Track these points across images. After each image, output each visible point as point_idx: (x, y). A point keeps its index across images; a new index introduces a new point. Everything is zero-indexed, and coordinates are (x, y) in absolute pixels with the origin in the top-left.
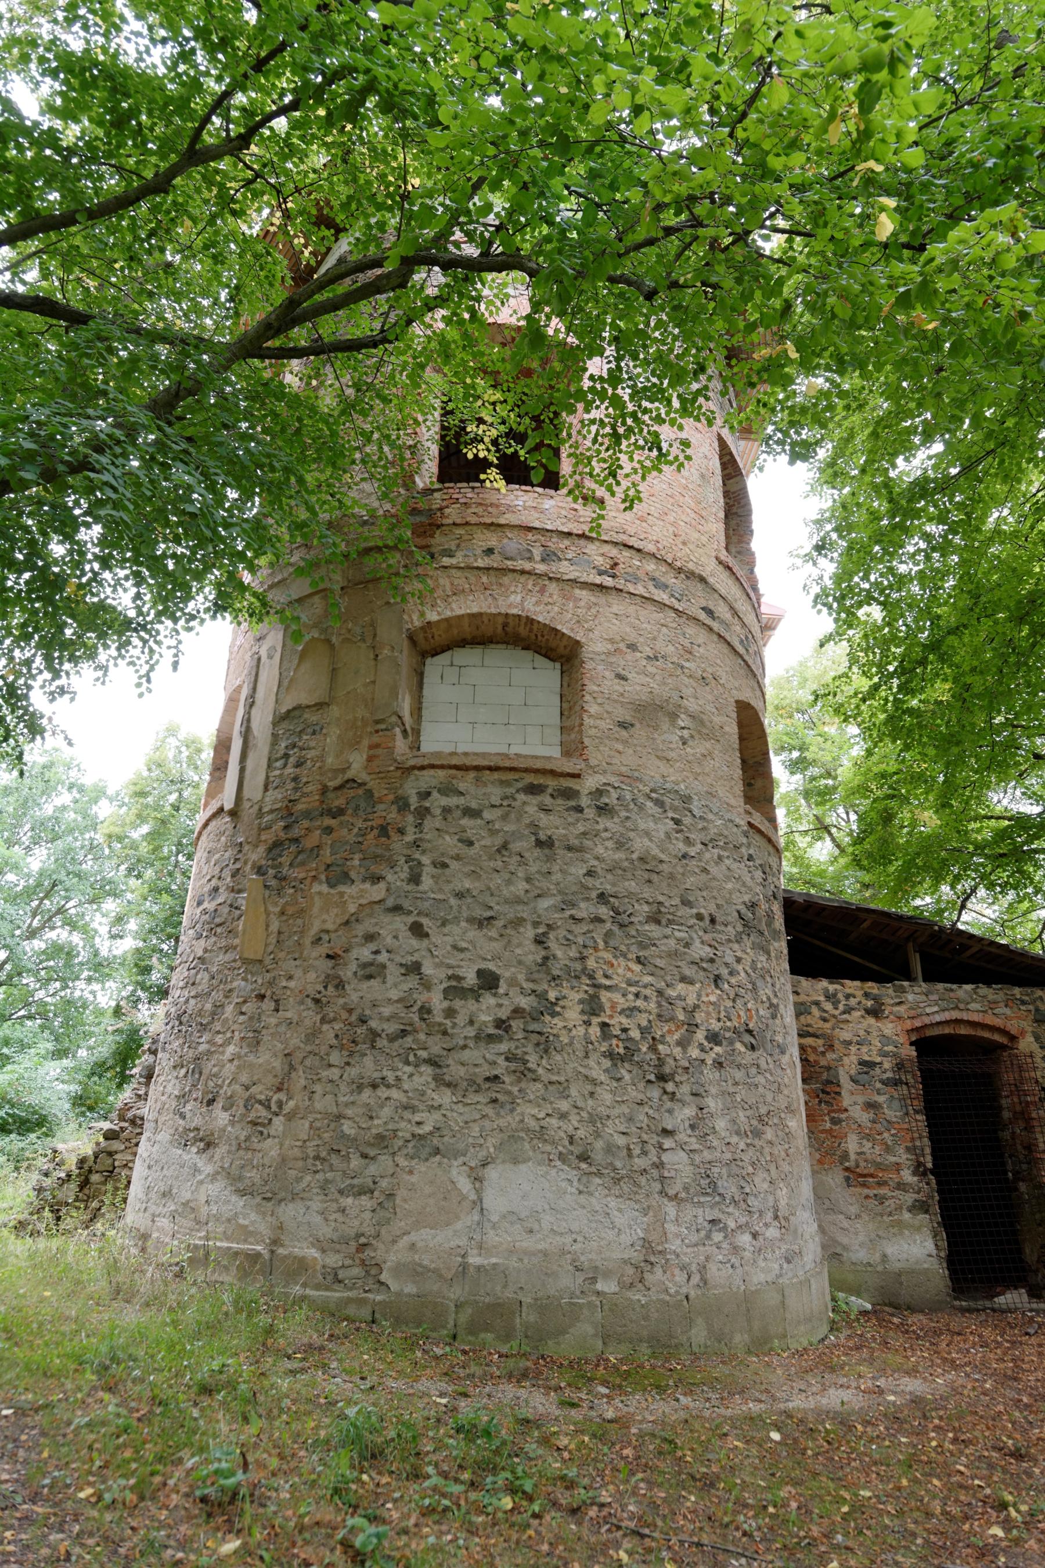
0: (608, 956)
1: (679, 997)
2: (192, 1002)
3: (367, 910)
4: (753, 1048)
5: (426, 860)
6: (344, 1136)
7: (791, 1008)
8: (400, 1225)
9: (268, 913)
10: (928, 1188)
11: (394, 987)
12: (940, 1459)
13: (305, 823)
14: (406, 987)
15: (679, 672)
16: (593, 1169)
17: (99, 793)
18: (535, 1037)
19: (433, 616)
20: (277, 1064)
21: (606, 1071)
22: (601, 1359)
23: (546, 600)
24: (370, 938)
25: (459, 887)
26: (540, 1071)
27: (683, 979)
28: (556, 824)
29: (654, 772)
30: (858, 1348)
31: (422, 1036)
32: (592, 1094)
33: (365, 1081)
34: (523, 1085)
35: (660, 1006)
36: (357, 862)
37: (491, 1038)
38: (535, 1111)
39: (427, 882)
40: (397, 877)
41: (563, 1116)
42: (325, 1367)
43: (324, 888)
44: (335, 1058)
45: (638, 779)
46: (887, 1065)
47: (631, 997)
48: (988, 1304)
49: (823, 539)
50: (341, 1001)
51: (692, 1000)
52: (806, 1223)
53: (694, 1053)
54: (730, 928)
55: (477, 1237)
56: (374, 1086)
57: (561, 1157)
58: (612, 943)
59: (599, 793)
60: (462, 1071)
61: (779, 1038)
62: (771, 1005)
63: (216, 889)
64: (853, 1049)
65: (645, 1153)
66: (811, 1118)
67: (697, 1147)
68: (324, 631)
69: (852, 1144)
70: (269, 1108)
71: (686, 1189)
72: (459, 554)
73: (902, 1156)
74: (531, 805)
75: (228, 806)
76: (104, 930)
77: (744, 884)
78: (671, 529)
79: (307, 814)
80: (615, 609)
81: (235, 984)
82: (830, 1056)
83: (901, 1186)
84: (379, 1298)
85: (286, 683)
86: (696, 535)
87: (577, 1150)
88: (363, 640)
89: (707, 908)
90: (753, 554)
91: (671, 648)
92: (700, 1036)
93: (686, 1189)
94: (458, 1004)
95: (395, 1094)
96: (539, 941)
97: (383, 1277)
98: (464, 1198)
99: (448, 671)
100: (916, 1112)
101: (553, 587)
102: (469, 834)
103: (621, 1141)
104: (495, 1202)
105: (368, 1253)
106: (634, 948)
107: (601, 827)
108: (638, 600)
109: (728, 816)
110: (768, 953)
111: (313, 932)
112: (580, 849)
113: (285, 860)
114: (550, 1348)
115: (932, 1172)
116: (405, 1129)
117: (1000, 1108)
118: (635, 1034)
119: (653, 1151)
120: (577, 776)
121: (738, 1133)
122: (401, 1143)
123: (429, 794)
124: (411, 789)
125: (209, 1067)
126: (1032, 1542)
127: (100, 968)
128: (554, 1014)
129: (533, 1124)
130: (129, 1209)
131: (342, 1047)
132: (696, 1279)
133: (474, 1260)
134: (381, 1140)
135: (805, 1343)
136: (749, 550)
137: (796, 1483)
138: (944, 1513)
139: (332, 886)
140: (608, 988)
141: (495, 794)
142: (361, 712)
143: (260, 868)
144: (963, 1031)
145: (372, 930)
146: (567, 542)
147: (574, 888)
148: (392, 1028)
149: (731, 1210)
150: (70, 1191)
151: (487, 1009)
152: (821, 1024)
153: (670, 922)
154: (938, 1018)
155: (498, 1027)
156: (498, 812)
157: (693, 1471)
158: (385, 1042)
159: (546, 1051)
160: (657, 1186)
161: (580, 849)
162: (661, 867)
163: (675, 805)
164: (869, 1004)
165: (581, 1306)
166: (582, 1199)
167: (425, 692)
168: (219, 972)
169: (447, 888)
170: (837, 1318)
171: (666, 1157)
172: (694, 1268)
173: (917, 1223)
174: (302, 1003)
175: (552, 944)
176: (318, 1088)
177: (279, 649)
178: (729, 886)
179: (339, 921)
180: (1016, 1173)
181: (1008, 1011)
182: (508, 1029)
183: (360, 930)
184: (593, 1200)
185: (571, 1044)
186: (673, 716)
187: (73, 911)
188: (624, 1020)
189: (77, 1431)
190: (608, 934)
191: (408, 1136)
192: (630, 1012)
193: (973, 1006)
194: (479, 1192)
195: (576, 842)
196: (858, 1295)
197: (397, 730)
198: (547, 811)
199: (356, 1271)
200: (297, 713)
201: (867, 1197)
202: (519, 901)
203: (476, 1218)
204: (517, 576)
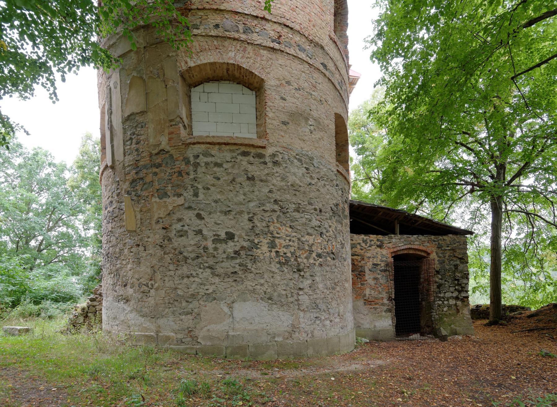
2: (111, 249)
3: (177, 209)
4: (334, 259)
5: (200, 186)
6: (178, 295)
9: (135, 211)
10: (392, 305)
12: (385, 382)
13: (145, 171)
15: (310, 97)
16: (273, 302)
17: (63, 168)
18: (250, 257)
19: (192, 64)
20: (149, 270)
21: (278, 268)
22: (277, 361)
23: (247, 55)
24: (180, 220)
25: (215, 198)
26: (253, 269)
27: (308, 234)
28: (255, 170)
29: (297, 145)
30: (363, 353)
31: (205, 258)
33: (185, 275)
34: (246, 274)
35: (299, 244)
36: (170, 188)
37: (232, 258)
38: (251, 284)
39: (201, 196)
40: (188, 194)
41: (262, 285)
42: (178, 369)
43: (157, 200)
44: (171, 267)
46: (382, 265)
47: (287, 241)
48: (407, 338)
49: (380, 30)
50: (171, 246)
51: (311, 242)
52: (349, 317)
53: (312, 261)
54: (327, 214)
55: (232, 326)
56: (188, 277)
58: (280, 220)
59: (274, 155)
60: (222, 270)
61: (344, 256)
62: (342, 243)
63: (111, 202)
64: (371, 259)
66: (354, 284)
67: (311, 293)
68: (139, 72)
69: (367, 292)
70: (148, 286)
71: (307, 307)
72: (202, 27)
73: (384, 295)
74: (244, 161)
75: (109, 164)
76: (81, 227)
77: (334, 196)
78: (308, 17)
79: (145, 167)
80: (280, 62)
81: (127, 241)
83: (383, 304)
84: (198, 347)
85: (125, 101)
86: (320, 21)
87: (267, 296)
88: (159, 77)
89: (318, 206)
90: (347, 37)
91: (306, 84)
92: (314, 255)
93: (307, 307)
94: (218, 245)
95: (196, 279)
96: (250, 220)
97: (199, 341)
98: (226, 314)
99: (202, 94)
100: (391, 280)
101: (250, 48)
102: (218, 175)
103: (284, 293)
105: (192, 333)
106: (289, 222)
107: (275, 171)
108: (291, 57)
110: (342, 224)
111: (155, 219)
114: (259, 358)
115: (394, 300)
117: (420, 278)
118: (289, 255)
119: (296, 296)
120: (264, 147)
121: (326, 289)
122: (201, 296)
123: (198, 156)
125: (122, 273)
126: (410, 402)
127: (83, 242)
128: (257, 248)
129: (250, 288)
130: (103, 324)
131: (174, 263)
132: (310, 335)
133: (231, 333)
135: (346, 352)
136: (345, 35)
137: (338, 391)
138: (384, 396)
139: (161, 199)
140: (278, 238)
141: (228, 156)
143: (128, 192)
144: (411, 252)
145: (180, 217)
146: (256, 22)
147: (264, 198)
148: (193, 255)
149: (323, 313)
150: (81, 319)
151: (231, 247)
152: (360, 251)
153: (303, 211)
154: (403, 248)
155: (235, 254)
156: (230, 165)
157: (305, 390)
158: (191, 261)
159: (255, 262)
160: (297, 307)
162: (300, 189)
163: (307, 162)
164: (379, 243)
165: (270, 346)
166: (269, 312)
167: (193, 106)
168: (119, 236)
169: (210, 198)
170: (357, 345)
171: (300, 297)
172: (309, 332)
173: (387, 315)
175: (256, 221)
176: (166, 278)
177: (119, 83)
178: (328, 197)
179: (165, 214)
180: (422, 299)
181: (428, 244)
183: (175, 217)
184: (274, 312)
185: (264, 259)
186: (307, 119)
187: (65, 219)
188: (285, 250)
189: (82, 393)
190: (278, 217)
191: (203, 294)
192: (287, 247)
193: (416, 243)
195: (264, 178)
196: (365, 338)
197: (181, 125)
199: (189, 339)
200: (132, 117)
201: (371, 308)
202: (241, 204)
203: (231, 320)
204: (231, 41)
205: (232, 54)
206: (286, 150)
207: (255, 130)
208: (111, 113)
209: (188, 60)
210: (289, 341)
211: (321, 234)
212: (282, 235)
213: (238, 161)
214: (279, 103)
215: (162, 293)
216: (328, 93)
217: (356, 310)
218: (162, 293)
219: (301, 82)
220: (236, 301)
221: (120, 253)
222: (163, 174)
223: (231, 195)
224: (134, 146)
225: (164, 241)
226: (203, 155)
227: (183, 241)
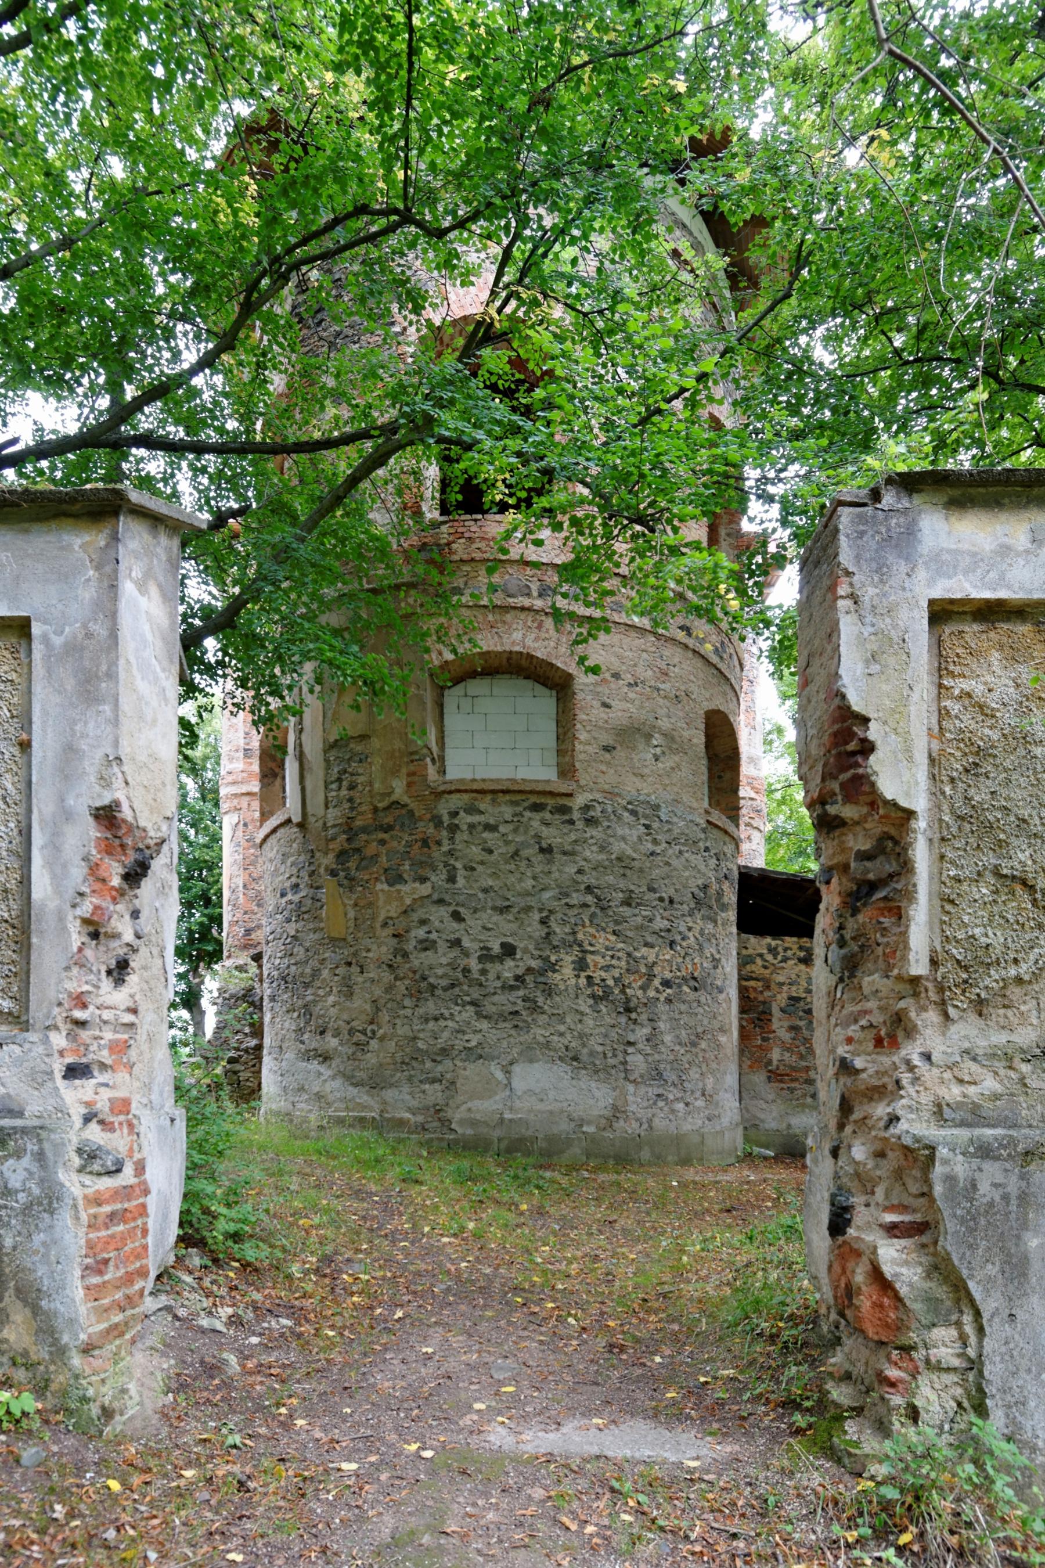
0: (592, 930)
6: (419, 1050)
8: (460, 1098)
11: (442, 957)
13: (363, 837)
20: (368, 1007)
23: (543, 635)
24: (423, 922)
25: (484, 885)
29: (632, 787)
37: (512, 988)
39: (461, 882)
40: (438, 878)
41: (561, 1034)
43: (385, 887)
44: (407, 1002)
45: (618, 795)
51: (651, 959)
53: (652, 993)
56: (436, 1019)
57: (560, 1058)
59: (587, 808)
60: (494, 1009)
65: (615, 1056)
69: (776, 1055)
72: (467, 592)
74: (534, 820)
75: (296, 819)
79: (364, 830)
82: (767, 994)
85: (330, 714)
87: (571, 1054)
91: (650, 673)
92: (657, 982)
95: (450, 1023)
96: (543, 922)
98: (499, 1082)
99: (463, 700)
102: (490, 844)
103: (600, 1049)
104: (519, 1084)
109: (690, 817)
112: (572, 853)
113: (352, 864)
116: (459, 1044)
124: (443, 810)
125: (317, 1010)
128: (554, 971)
129: (541, 1039)
131: (411, 996)
132: (645, 1126)
133: (508, 1116)
134: (444, 1052)
139: (391, 885)
141: (507, 812)
142: (398, 744)
148: (444, 982)
151: (509, 969)
156: (511, 827)
161: (572, 853)
163: (644, 812)
164: (802, 954)
167: (446, 722)
169: (475, 885)
175: (553, 924)
182: (523, 982)
183: (415, 917)
186: (649, 737)
188: (603, 974)
190: (593, 916)
192: (607, 968)
198: (547, 825)
199: (436, 1124)
202: (528, 894)
205: (517, 636)
207: (554, 761)
208: (301, 731)
210: (606, 1134)
211: (672, 944)
212: (598, 947)
213: (524, 820)
214: (598, 713)
215: (391, 1045)
217: (743, 1091)
218: (391, 1045)
221: (313, 976)
222: (395, 844)
223: (512, 879)
224: (344, 792)
227: (428, 958)
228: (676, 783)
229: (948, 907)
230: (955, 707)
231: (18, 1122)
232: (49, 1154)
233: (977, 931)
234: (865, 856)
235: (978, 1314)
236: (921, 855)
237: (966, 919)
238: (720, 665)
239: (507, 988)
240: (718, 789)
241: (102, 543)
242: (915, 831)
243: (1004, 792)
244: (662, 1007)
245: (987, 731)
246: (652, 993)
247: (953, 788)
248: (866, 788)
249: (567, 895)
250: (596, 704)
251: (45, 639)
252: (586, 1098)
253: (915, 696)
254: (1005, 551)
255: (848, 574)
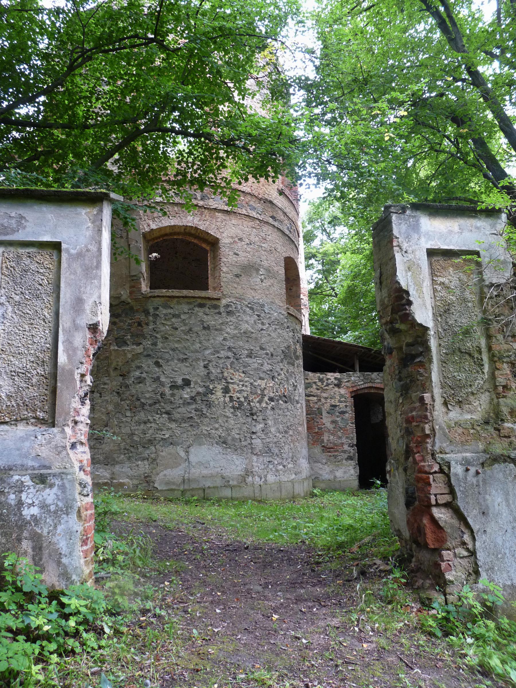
0: (232, 371)
1: (259, 385)
4: (286, 402)
5: (158, 336)
7: (303, 386)
10: (353, 451)
11: (149, 387)
14: (154, 386)
18: (205, 403)
21: (232, 413)
23: (203, 218)
24: (139, 367)
26: (208, 414)
27: (261, 378)
29: (251, 296)
32: (227, 421)
34: (202, 419)
36: (129, 337)
37: (189, 404)
38: (206, 428)
39: (160, 345)
41: (217, 429)
45: (244, 299)
47: (240, 386)
50: (129, 392)
51: (263, 386)
53: (264, 405)
54: (279, 357)
56: (145, 423)
57: (217, 443)
58: (233, 366)
59: (227, 306)
60: (178, 416)
62: (294, 385)
64: (329, 400)
65: (246, 440)
69: (325, 438)
74: (200, 312)
77: (285, 339)
83: (345, 452)
87: (221, 440)
92: (266, 399)
94: (176, 391)
95: (153, 425)
96: (205, 367)
102: (176, 325)
103: (237, 436)
106: (242, 368)
108: (243, 217)
109: (279, 311)
118: (242, 399)
123: (158, 308)
128: (212, 394)
129: (206, 432)
132: (263, 480)
134: (151, 442)
140: (232, 383)
141: (185, 308)
147: (218, 346)
148: (150, 402)
152: (316, 391)
153: (256, 357)
154: (363, 387)
159: (210, 407)
160: (250, 451)
164: (336, 382)
174: (111, 393)
178: (279, 340)
185: (219, 404)
186: (258, 270)
188: (238, 395)
190: (232, 363)
194: (188, 456)
206: (239, 300)
209: (151, 223)
211: (273, 378)
212: (235, 380)
216: (277, 241)
219: (252, 238)
220: (192, 445)
225: (121, 387)
226: (162, 307)
228: (268, 291)
229: (444, 365)
230: (439, 288)
231: (49, 471)
232: (67, 486)
233: (456, 374)
234: (408, 345)
235: (472, 532)
236: (433, 343)
237: (451, 369)
238: (290, 235)
239: (186, 403)
240: (290, 296)
241: (95, 213)
242: (430, 335)
243: (460, 320)
244: (269, 412)
245: (451, 297)
246: (264, 405)
247: (441, 319)
248: (410, 318)
249: (218, 352)
250: (231, 253)
251: (67, 250)
252: (234, 465)
253: (425, 284)
254: (451, 232)
255: (397, 238)
